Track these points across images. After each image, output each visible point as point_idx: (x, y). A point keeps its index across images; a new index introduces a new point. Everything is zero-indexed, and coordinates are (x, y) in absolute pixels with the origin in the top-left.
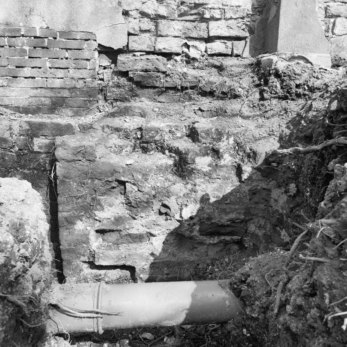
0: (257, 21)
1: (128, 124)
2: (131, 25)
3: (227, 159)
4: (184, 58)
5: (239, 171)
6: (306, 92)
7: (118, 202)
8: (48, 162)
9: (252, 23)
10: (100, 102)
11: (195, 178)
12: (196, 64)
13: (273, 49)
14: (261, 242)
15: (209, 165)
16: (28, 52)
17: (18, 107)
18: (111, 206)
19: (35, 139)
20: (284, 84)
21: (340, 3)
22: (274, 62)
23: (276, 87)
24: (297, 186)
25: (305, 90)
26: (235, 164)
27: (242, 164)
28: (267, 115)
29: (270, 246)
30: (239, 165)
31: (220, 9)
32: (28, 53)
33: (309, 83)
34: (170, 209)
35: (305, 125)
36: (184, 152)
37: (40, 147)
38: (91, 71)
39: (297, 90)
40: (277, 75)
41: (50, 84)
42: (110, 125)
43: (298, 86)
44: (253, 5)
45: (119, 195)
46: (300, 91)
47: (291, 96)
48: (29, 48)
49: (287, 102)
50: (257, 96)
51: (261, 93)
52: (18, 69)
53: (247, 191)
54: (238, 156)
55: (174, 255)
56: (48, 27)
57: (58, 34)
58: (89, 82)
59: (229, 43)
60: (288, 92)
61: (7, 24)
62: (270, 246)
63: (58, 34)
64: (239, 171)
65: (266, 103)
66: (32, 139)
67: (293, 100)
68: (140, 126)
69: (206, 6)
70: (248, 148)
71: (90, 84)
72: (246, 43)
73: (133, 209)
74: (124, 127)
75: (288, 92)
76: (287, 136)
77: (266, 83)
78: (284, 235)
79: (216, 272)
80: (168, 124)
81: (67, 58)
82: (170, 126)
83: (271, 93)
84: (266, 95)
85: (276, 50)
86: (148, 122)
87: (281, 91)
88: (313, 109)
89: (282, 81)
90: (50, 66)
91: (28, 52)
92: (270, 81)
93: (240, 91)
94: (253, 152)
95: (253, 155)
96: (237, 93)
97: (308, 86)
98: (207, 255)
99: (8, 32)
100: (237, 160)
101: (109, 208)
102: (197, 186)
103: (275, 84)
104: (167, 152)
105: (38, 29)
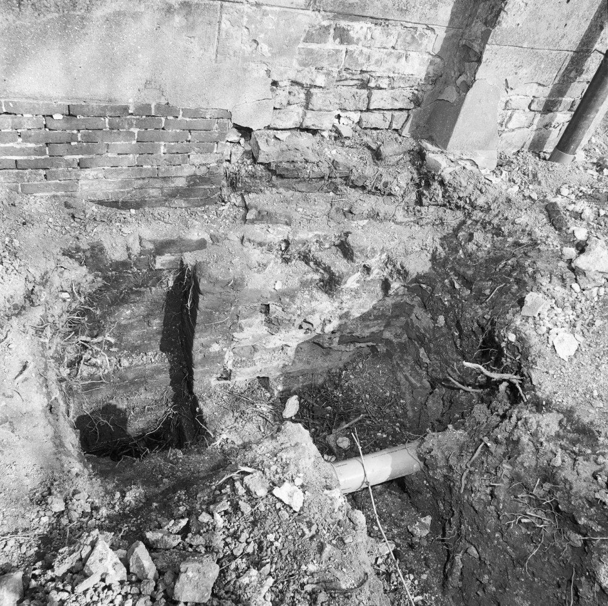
0: (428, 93)
1: (272, 236)
2: (278, 99)
3: (376, 273)
4: (333, 134)
5: (386, 285)
6: (467, 206)
7: (258, 320)
8: (68, 210)
9: (421, 93)
10: (225, 190)
11: (343, 296)
12: (347, 142)
13: (442, 142)
14: (395, 350)
15: (358, 282)
16: (136, 135)
17: (117, 202)
18: (250, 326)
19: (158, 257)
20: (447, 194)
21: (523, 97)
22: (442, 168)
23: (438, 195)
24: (446, 320)
25: (466, 202)
26: (383, 278)
27: (390, 279)
28: (421, 222)
29: (405, 357)
30: (386, 280)
31: (389, 77)
32: (136, 137)
33: (472, 197)
34: (312, 325)
35: (462, 256)
36: (337, 275)
37: (163, 265)
38: (218, 155)
39: (458, 201)
40: (442, 183)
41: (163, 173)
42: (252, 239)
43: (459, 198)
44: (428, 74)
45: (260, 314)
46: (461, 203)
47: (450, 205)
48: (138, 130)
49: (445, 211)
50: (414, 198)
51: (420, 195)
52: (120, 156)
53: (390, 305)
54: (386, 269)
55: (308, 363)
56: (168, 104)
57: (181, 113)
58: (214, 167)
59: (388, 115)
60: (449, 202)
61: (110, 101)
62: (405, 357)
63: (181, 113)
64: (386, 285)
65: (423, 209)
66: (154, 257)
67: (451, 209)
68: (286, 238)
69: (374, 74)
70: (399, 263)
71: (214, 171)
72: (408, 117)
73: (272, 326)
74: (268, 241)
75: (449, 202)
76: (441, 258)
77: (428, 185)
78: (423, 354)
79: (350, 379)
80: (316, 233)
81: (189, 141)
82: (319, 236)
83: (431, 200)
84: (424, 201)
85: (445, 147)
86: (295, 233)
87: (442, 199)
88: (473, 241)
89: (446, 191)
90: (165, 151)
91: (136, 135)
92: (433, 187)
93: (396, 190)
94: (405, 271)
95: (403, 273)
96: (393, 193)
97: (470, 200)
98: (340, 360)
99: (111, 111)
100: (385, 274)
101: (249, 328)
102: (344, 304)
103: (437, 192)
104: (312, 263)
105: (153, 106)
